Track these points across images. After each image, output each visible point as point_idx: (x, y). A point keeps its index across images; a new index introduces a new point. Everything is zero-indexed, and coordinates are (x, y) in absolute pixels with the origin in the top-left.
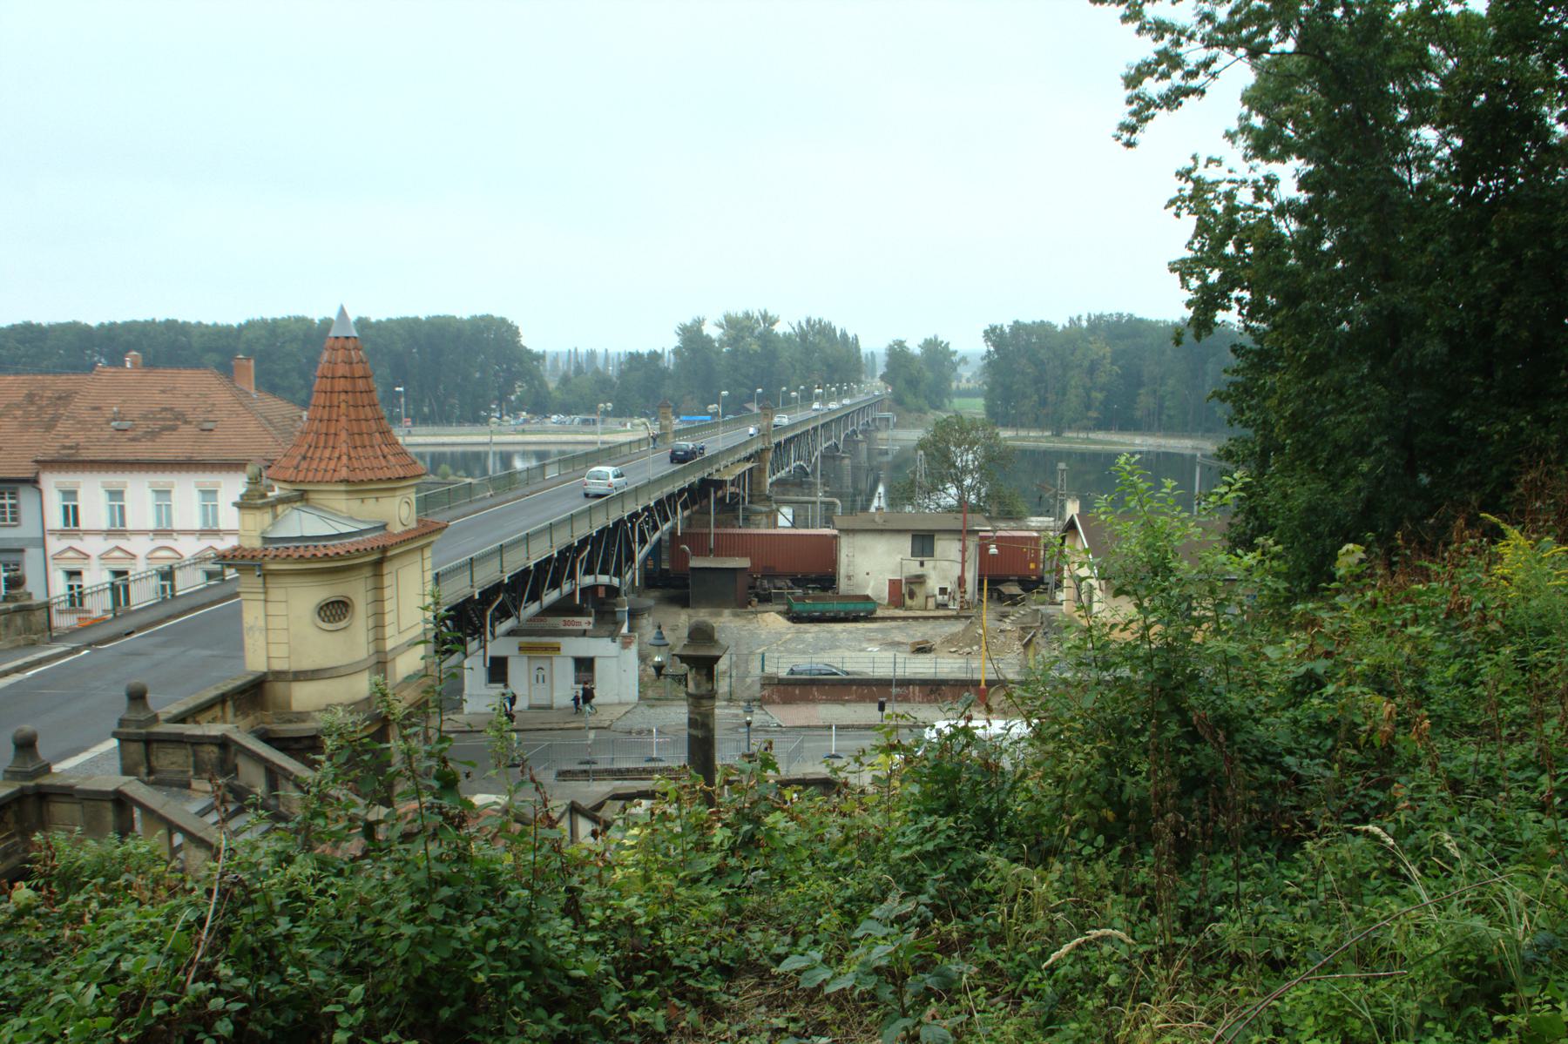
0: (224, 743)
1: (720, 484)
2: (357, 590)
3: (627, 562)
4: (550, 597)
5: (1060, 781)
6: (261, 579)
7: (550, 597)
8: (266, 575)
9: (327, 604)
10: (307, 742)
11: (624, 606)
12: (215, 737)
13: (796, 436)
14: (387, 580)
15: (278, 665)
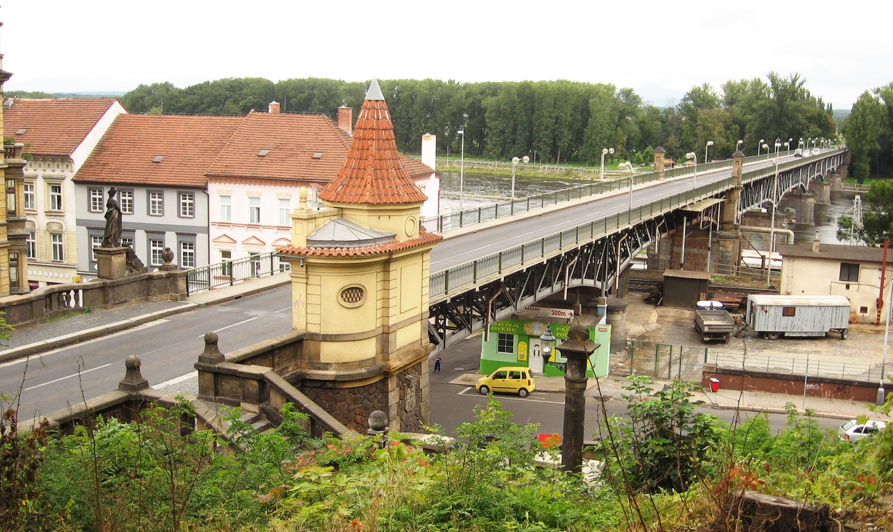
0: (262, 380)
1: (693, 215)
2: (370, 281)
3: (610, 270)
4: (543, 293)
5: (643, 455)
6: (304, 269)
7: (543, 293)
8: (308, 266)
9: (348, 289)
10: (319, 384)
11: (605, 302)
12: (256, 375)
13: (765, 179)
14: (392, 275)
15: (313, 329)
